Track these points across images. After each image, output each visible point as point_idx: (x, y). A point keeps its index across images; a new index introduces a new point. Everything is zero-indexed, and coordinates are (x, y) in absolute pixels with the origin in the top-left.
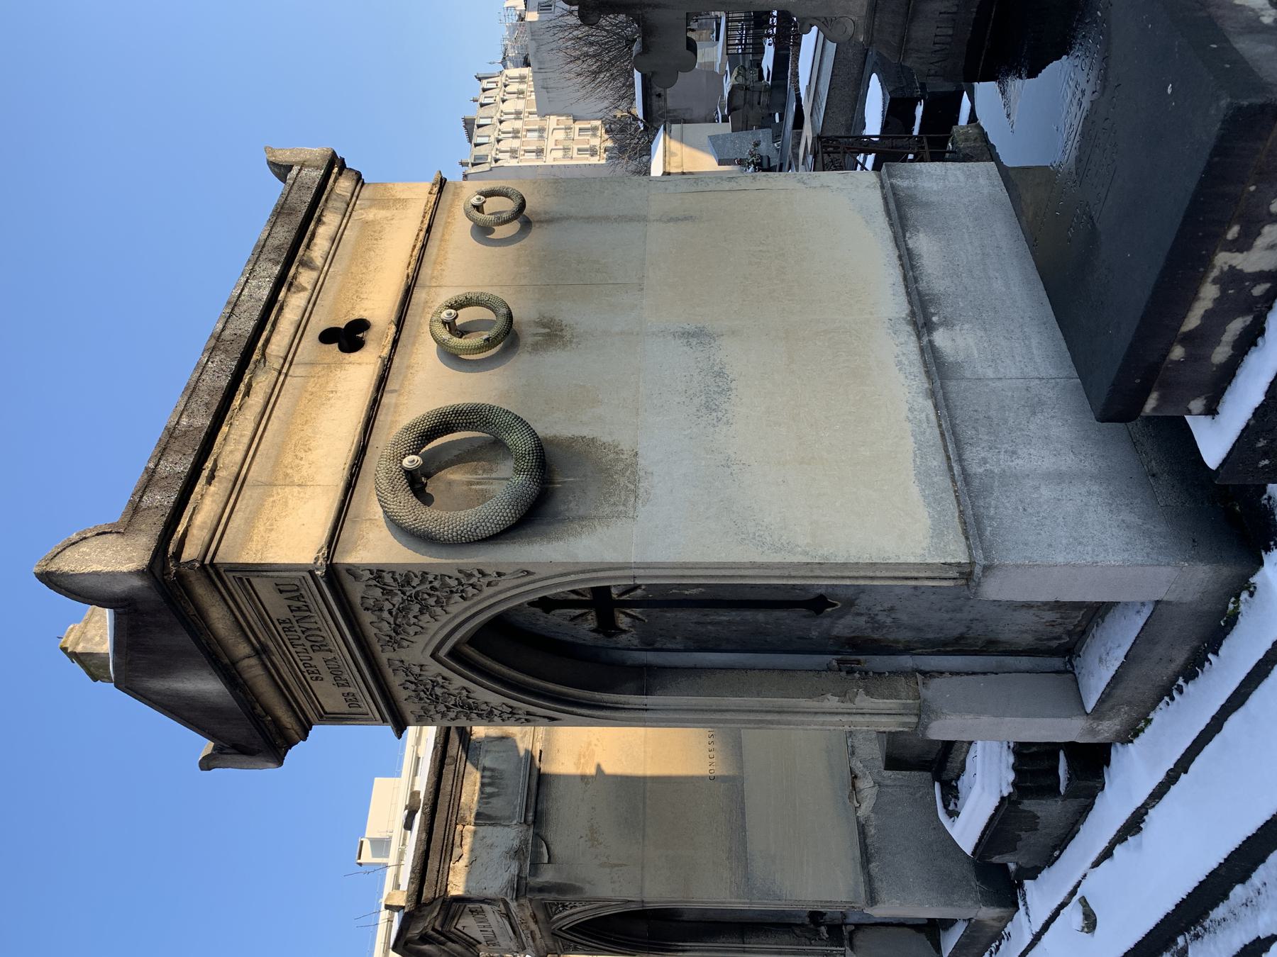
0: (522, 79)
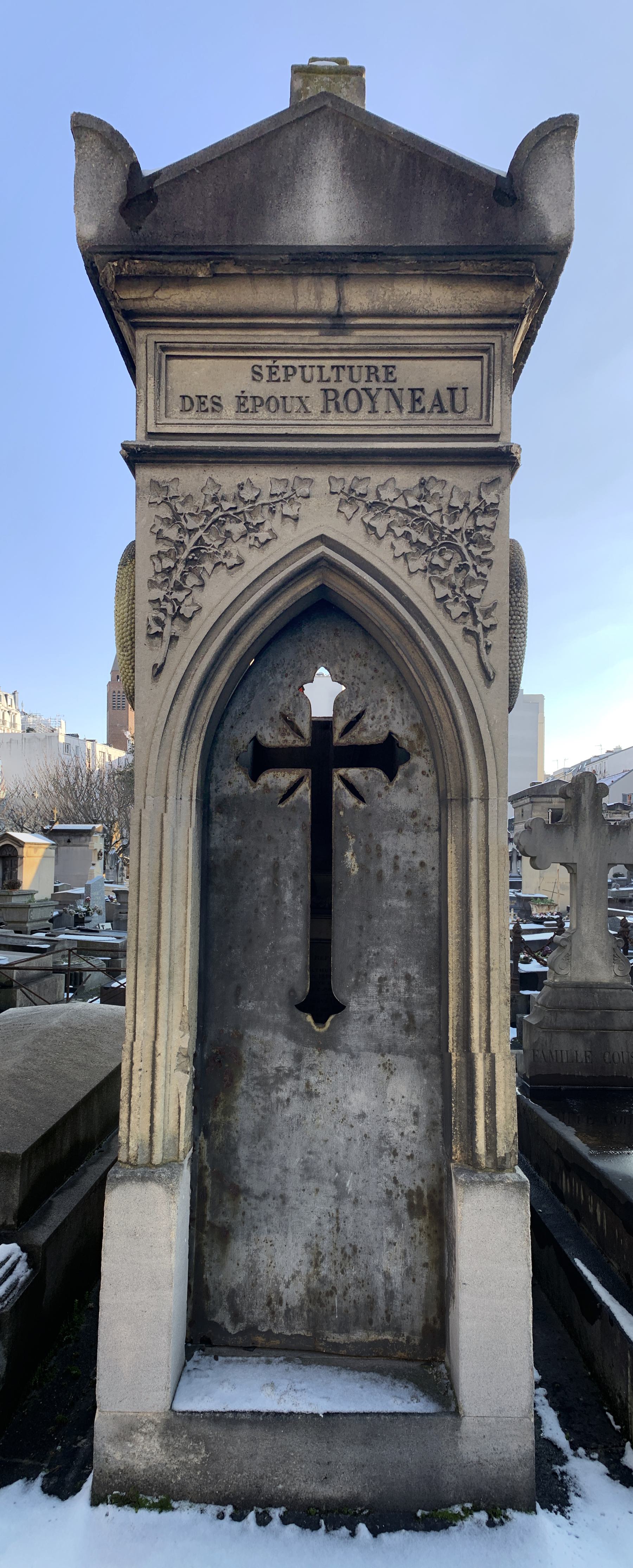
0: (14, 725)
